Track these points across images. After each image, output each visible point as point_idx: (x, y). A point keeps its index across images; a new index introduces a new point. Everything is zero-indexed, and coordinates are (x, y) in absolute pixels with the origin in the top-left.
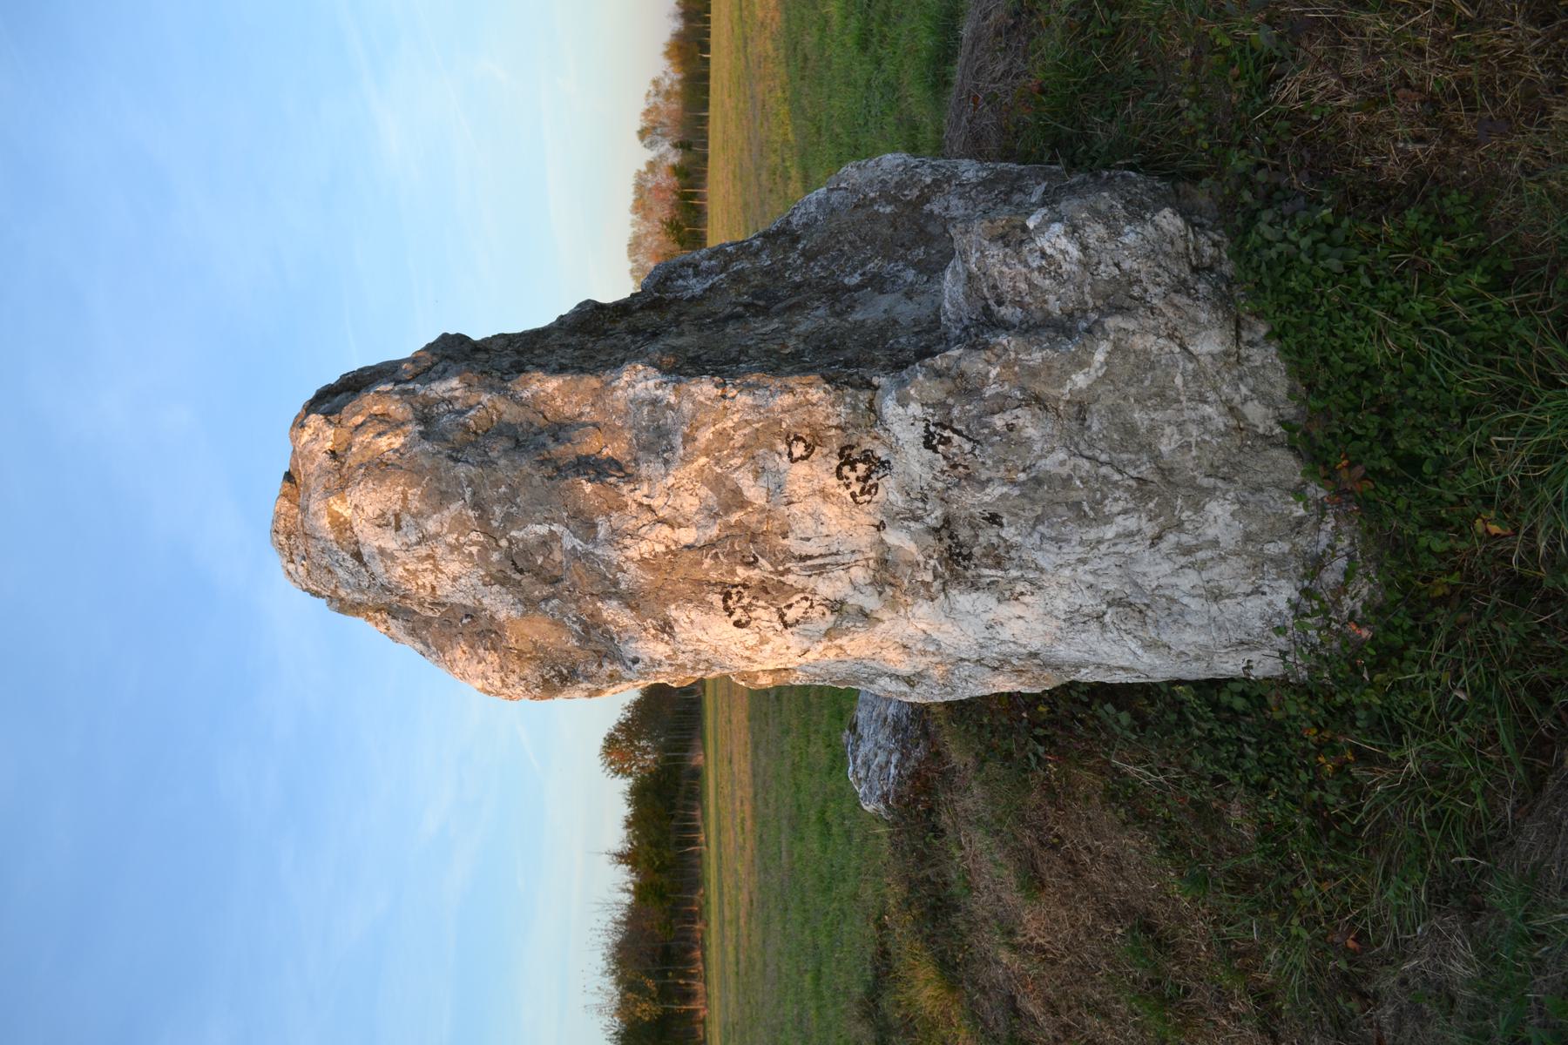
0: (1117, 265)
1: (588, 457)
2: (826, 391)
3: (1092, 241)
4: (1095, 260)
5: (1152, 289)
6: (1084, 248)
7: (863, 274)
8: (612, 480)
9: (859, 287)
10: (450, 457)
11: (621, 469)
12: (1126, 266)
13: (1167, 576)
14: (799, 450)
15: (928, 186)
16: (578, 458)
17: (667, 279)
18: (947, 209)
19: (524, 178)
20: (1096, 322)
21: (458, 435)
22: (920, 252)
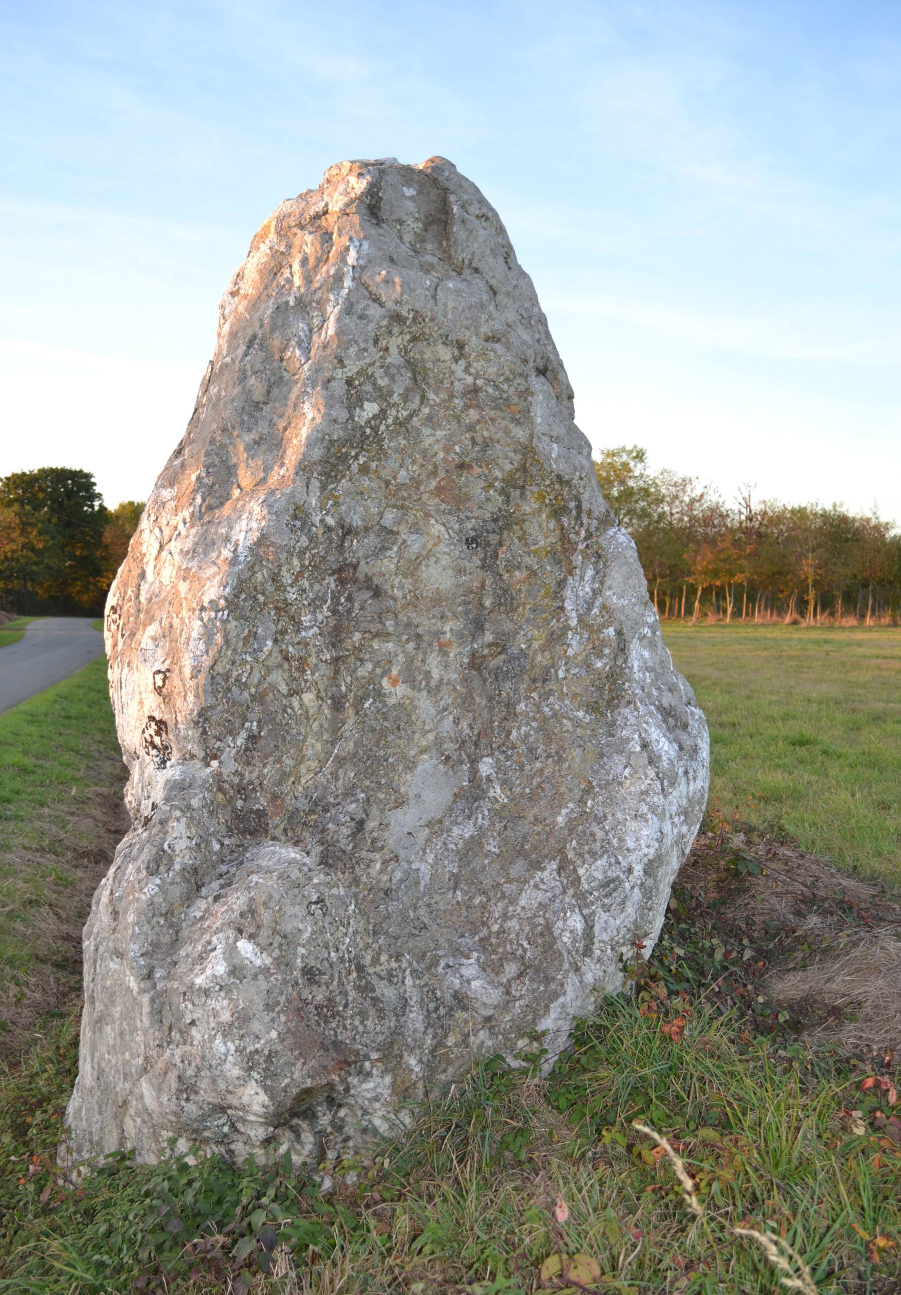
0: (193, 1023)
1: (236, 475)
2: (192, 710)
3: (212, 1003)
4: (196, 1002)
5: (178, 1052)
6: (207, 992)
7: (489, 779)
8: (199, 500)
9: (474, 771)
10: (254, 337)
11: (210, 508)
12: (194, 1031)
13: (175, 1028)
14: (159, 678)
15: (575, 870)
16: (235, 466)
17: (599, 556)
18: (536, 886)
19: (737, 368)
20: (154, 986)
21: (276, 342)
22: (492, 847)
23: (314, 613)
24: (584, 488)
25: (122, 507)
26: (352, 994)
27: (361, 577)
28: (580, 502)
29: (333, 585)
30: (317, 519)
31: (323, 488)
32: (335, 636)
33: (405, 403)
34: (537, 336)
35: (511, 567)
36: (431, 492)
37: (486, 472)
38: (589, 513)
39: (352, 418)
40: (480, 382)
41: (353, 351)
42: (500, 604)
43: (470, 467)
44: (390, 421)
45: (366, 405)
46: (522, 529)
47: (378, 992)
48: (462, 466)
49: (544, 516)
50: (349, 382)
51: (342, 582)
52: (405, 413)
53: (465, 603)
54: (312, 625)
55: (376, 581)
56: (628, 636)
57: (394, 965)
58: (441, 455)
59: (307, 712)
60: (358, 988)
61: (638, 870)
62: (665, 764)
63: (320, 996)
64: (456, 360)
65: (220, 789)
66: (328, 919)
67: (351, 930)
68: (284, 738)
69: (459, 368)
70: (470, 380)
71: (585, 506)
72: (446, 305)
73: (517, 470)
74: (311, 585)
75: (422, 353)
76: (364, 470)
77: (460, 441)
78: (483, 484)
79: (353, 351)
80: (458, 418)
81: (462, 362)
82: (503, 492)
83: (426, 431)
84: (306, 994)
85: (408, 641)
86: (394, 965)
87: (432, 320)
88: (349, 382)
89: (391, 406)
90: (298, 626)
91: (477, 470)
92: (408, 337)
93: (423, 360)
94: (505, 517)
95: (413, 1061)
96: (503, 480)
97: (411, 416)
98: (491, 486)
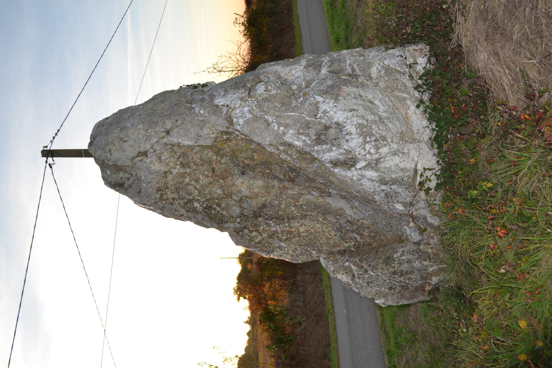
23: (271, 226)
24: (217, 130)
25: (237, 243)
26: (402, 279)
27: (258, 211)
28: (223, 132)
29: (262, 219)
30: (238, 225)
31: (226, 222)
32: (280, 219)
33: (192, 193)
34: (153, 133)
35: (252, 159)
36: (224, 182)
37: (214, 162)
38: (227, 128)
39: (201, 213)
40: (178, 163)
41: (177, 213)
42: (268, 167)
43: (213, 168)
44: (200, 198)
45: (195, 206)
46: (237, 151)
47: (404, 270)
48: (213, 171)
49: (230, 144)
50: (188, 211)
51: (260, 216)
52: (196, 192)
53: (268, 178)
54: (275, 227)
55: (260, 206)
56: (282, 141)
57: (397, 262)
58: (210, 179)
59: (306, 230)
60: (401, 276)
61: (383, 187)
62: (341, 157)
63: (399, 288)
64: (171, 173)
65: (329, 258)
66: (374, 282)
67: (380, 275)
68: (314, 243)
69: (175, 172)
70: (178, 167)
71: (225, 129)
72: (151, 178)
73: (212, 150)
74: (261, 226)
75: (172, 185)
76: (218, 205)
77: (203, 171)
78: (219, 164)
79: (177, 213)
80: (194, 170)
81: (172, 170)
82: (222, 156)
83: (201, 182)
84: (397, 291)
85: (282, 197)
86: (397, 262)
87: (158, 183)
88: (188, 211)
89: (194, 198)
90: (276, 232)
91: (214, 165)
92: (167, 190)
93: (174, 185)
94: (232, 158)
95: (431, 269)
96: (217, 156)
97: (196, 189)
98: (220, 161)
